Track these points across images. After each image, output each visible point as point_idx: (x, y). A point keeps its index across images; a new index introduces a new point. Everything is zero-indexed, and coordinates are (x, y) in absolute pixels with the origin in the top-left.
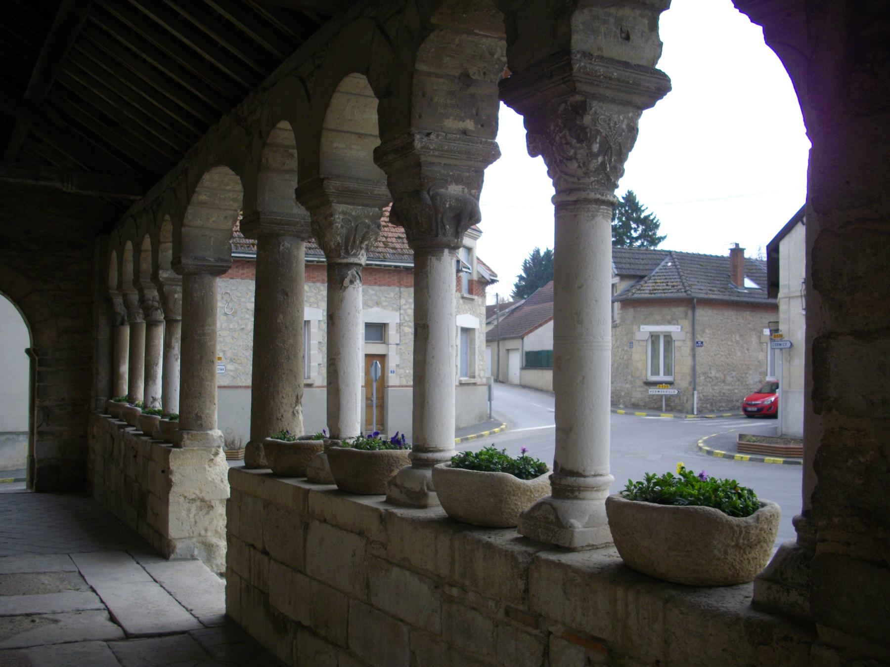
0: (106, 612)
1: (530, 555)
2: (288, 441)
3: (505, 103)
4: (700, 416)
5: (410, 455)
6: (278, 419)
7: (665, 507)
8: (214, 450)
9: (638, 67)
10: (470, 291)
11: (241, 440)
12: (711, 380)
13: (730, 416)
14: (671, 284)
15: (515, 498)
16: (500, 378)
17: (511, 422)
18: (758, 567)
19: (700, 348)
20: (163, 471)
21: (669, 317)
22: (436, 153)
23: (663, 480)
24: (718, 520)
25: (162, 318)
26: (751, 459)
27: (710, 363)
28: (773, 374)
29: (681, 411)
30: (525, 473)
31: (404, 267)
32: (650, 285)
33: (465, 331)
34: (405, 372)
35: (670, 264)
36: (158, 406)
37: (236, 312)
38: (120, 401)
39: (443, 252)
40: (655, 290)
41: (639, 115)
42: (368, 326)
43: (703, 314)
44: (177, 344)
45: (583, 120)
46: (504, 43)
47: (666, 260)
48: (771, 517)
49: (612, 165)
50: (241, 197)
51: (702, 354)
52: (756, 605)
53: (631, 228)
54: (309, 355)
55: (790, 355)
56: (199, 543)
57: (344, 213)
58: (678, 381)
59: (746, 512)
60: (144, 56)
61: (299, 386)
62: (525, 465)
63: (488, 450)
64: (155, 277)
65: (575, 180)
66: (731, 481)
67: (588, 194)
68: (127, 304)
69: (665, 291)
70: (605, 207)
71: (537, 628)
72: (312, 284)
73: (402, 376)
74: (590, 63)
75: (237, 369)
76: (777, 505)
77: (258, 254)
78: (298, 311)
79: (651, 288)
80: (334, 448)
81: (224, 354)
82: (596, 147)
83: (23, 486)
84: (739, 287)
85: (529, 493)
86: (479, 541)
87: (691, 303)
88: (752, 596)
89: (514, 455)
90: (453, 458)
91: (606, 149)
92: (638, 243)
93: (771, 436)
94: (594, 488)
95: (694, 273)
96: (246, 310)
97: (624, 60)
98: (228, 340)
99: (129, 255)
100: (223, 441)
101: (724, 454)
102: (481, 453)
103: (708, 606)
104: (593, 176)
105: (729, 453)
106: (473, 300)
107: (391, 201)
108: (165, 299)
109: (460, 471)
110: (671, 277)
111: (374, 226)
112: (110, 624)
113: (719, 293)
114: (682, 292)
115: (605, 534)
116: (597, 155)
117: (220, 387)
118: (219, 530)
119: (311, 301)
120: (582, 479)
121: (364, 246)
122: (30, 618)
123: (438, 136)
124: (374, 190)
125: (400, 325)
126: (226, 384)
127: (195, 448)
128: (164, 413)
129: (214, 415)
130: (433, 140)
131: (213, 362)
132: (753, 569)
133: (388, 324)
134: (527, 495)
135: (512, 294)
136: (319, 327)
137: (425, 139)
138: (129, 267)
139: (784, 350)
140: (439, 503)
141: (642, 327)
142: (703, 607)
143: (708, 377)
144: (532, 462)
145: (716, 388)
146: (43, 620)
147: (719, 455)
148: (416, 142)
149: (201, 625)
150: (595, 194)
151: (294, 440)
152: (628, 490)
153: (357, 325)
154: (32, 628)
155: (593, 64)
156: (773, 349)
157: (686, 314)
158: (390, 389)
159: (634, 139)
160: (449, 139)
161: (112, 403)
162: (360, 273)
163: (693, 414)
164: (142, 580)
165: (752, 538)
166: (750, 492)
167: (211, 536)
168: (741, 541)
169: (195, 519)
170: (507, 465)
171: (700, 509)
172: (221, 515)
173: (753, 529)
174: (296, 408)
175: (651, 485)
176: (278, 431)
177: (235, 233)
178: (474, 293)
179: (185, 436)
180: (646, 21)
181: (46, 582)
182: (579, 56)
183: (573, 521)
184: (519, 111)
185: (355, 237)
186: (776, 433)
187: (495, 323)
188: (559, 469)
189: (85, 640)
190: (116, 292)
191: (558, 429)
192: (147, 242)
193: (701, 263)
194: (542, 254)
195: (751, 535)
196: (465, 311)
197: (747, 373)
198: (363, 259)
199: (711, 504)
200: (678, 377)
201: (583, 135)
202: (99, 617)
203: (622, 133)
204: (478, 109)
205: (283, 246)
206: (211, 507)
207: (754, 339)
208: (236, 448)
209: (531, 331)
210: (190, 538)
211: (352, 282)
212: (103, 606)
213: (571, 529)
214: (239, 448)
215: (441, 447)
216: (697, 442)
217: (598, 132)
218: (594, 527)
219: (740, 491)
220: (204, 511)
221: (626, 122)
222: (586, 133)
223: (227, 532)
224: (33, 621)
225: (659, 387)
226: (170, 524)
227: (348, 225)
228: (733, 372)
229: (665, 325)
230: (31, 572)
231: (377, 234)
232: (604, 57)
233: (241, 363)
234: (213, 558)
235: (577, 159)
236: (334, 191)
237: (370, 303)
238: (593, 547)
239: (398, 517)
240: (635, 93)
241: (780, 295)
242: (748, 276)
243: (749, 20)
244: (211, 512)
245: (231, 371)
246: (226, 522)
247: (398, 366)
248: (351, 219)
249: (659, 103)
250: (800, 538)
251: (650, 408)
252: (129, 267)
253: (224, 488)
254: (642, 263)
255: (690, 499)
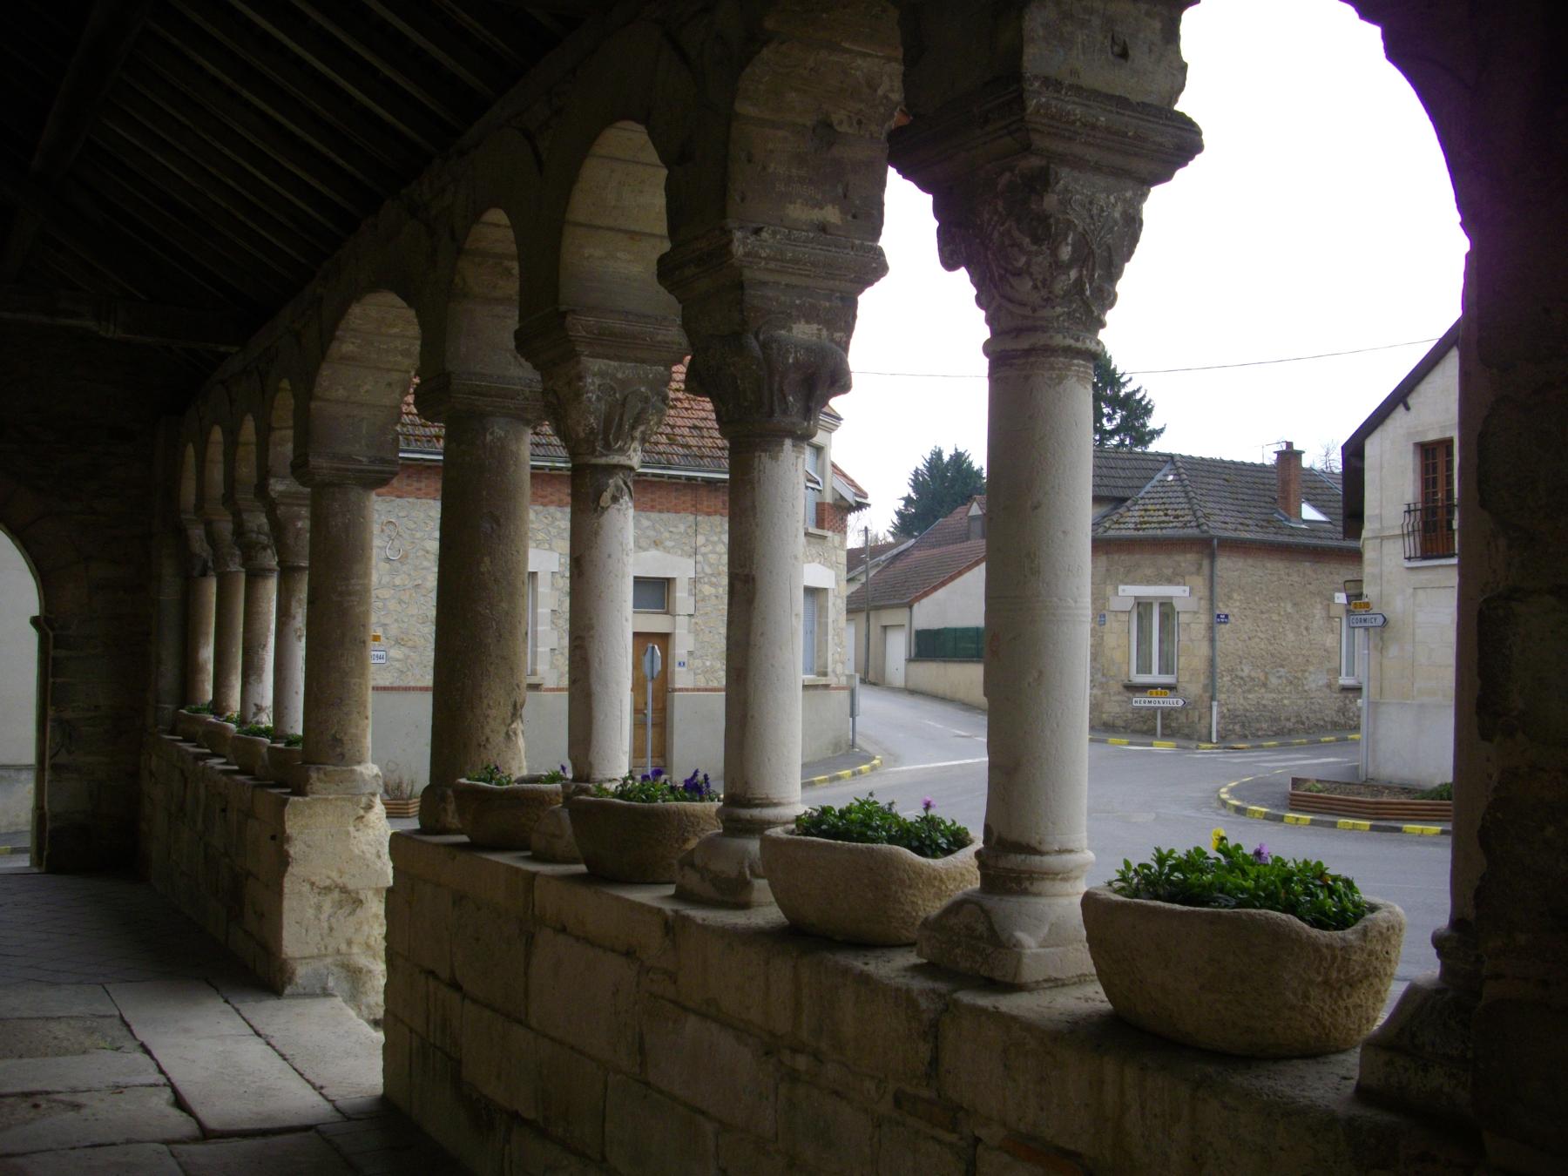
0: (169, 1090)
1: (940, 996)
2: (498, 784)
3: (899, 172)
4: (1222, 745)
5: (719, 811)
6: (480, 745)
7: (1194, 912)
8: (364, 800)
9: (1144, 106)
10: (820, 523)
11: (412, 782)
12: (1242, 683)
13: (1275, 746)
14: (1174, 513)
15: (911, 892)
16: (871, 676)
17: (890, 754)
18: (1364, 1021)
19: (1223, 626)
20: (273, 838)
21: (1169, 572)
22: (772, 265)
23: (1186, 861)
24: (1294, 936)
25: (275, 563)
26: (1313, 822)
27: (1240, 653)
28: (1350, 673)
29: (1188, 737)
30: (930, 846)
31: (704, 479)
32: (1136, 514)
33: (811, 592)
34: (704, 663)
35: (1170, 478)
36: (267, 720)
37: (406, 556)
38: (198, 711)
39: (783, 445)
40: (1146, 523)
41: (1144, 196)
42: (639, 581)
43: (1228, 566)
44: (300, 610)
45: (1043, 201)
46: (897, 68)
47: (1165, 470)
48: (1388, 930)
49: (1094, 284)
50: (416, 347)
51: (1227, 636)
52: (1364, 1093)
53: (1103, 415)
54: (535, 633)
55: (1382, 639)
56: (337, 966)
57: (602, 374)
58: (1184, 684)
59: (1342, 920)
60: (246, 94)
61: (518, 686)
62: (929, 831)
63: (862, 804)
64: (262, 489)
65: (1027, 311)
66: (1313, 863)
67: (1051, 337)
68: (212, 539)
69: (1162, 525)
70: (1082, 362)
71: (953, 1131)
72: (541, 508)
73: (699, 671)
74: (1056, 99)
75: (407, 657)
76: (1398, 909)
77: (446, 452)
78: (518, 552)
79: (1138, 520)
80: (581, 797)
81: (385, 630)
82: (1065, 253)
83: (24, 862)
84: (1293, 519)
85: (937, 883)
86: (846, 971)
87: (1208, 547)
88: (1357, 1078)
89: (910, 812)
90: (798, 818)
91: (1083, 256)
92: (1115, 441)
93: (1347, 781)
94: (1057, 874)
95: (1215, 493)
96: (423, 553)
97: (1117, 94)
98: (392, 605)
99: (216, 452)
100: (381, 783)
101: (1266, 813)
102: (849, 810)
103: (1275, 1094)
104: (1059, 305)
105: (1275, 811)
106: (824, 538)
107: (687, 355)
108: (279, 529)
109: (813, 841)
110: (1173, 500)
111: (655, 398)
112: (176, 1113)
113: (1258, 529)
114: (1192, 527)
115: (1080, 958)
116: (1069, 266)
117: (375, 689)
118: (373, 943)
119: (540, 538)
120: (1037, 858)
121: (637, 434)
122: (31, 1101)
123: (774, 233)
124: (658, 334)
125: (695, 581)
126: (387, 684)
127: (330, 797)
128: (276, 733)
129: (365, 738)
130: (765, 241)
131: (364, 642)
132: (1356, 1026)
133: (674, 579)
134: (934, 886)
135: (892, 530)
136: (553, 585)
137: (752, 238)
138: (217, 474)
139: (1371, 631)
140: (773, 899)
141: (1121, 588)
142: (1265, 1097)
143: (1237, 676)
144: (942, 827)
145: (1250, 696)
146: (53, 1104)
147: (1257, 815)
148: (736, 243)
149: (339, 1115)
150: (1064, 337)
151: (508, 783)
152: (1124, 878)
153: (623, 577)
154: (33, 1119)
155: (1062, 100)
156: (1352, 628)
157: (1200, 567)
158: (676, 693)
159: (1134, 239)
160: (794, 240)
161: (184, 715)
162: (630, 484)
163: (1211, 742)
164: (233, 1032)
165: (1354, 969)
166: (1349, 884)
167: (358, 954)
168: (1334, 975)
169: (330, 924)
170: (896, 832)
171: (1260, 915)
172: (376, 916)
173: (1355, 952)
174: (513, 726)
175: (1166, 870)
176: (480, 767)
177: (405, 416)
178: (826, 526)
179: (314, 775)
180: (1157, 25)
181: (61, 1035)
182: (1037, 84)
183: (1021, 935)
184: (924, 187)
185: (621, 419)
186: (1358, 776)
187: (863, 579)
188: (994, 840)
189: (128, 1142)
190: (194, 518)
191: (992, 766)
192: (249, 430)
193: (1224, 476)
194: (946, 458)
195: (1352, 963)
196: (810, 559)
197: (1305, 671)
198: (635, 458)
199: (1280, 907)
200: (1184, 678)
201: (1043, 230)
202: (155, 1100)
203: (1113, 227)
204: (847, 185)
205: (492, 434)
206: (359, 902)
207: (1318, 611)
208: (405, 796)
209: (926, 594)
210: (320, 957)
211: (615, 499)
212: (162, 1080)
213: (1016, 949)
214: (410, 798)
215: (775, 797)
216: (1217, 791)
217: (1070, 225)
218: (1058, 946)
219: (1330, 882)
220: (347, 909)
221: (1119, 207)
222: (1048, 227)
223: (387, 950)
224: (36, 1106)
225: (1151, 694)
226: (285, 934)
227: (610, 396)
228: (1281, 669)
229: (1161, 585)
230: (36, 1016)
231: (661, 413)
232: (1081, 88)
233: (415, 647)
234: (362, 993)
235: (1031, 275)
236: (584, 333)
237: (643, 543)
238: (1057, 983)
239: (698, 925)
240: (1136, 155)
241: (1365, 534)
242: (1308, 500)
243: (1356, 15)
244: (358, 910)
245: (397, 660)
246: (385, 928)
247: (691, 653)
248: (615, 385)
249: (1180, 174)
250: (1446, 971)
251: (1135, 732)
252: (217, 474)
253: (382, 869)
254: (1123, 475)
255: (1240, 896)
